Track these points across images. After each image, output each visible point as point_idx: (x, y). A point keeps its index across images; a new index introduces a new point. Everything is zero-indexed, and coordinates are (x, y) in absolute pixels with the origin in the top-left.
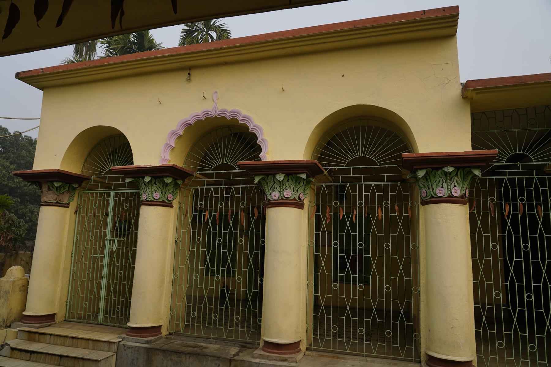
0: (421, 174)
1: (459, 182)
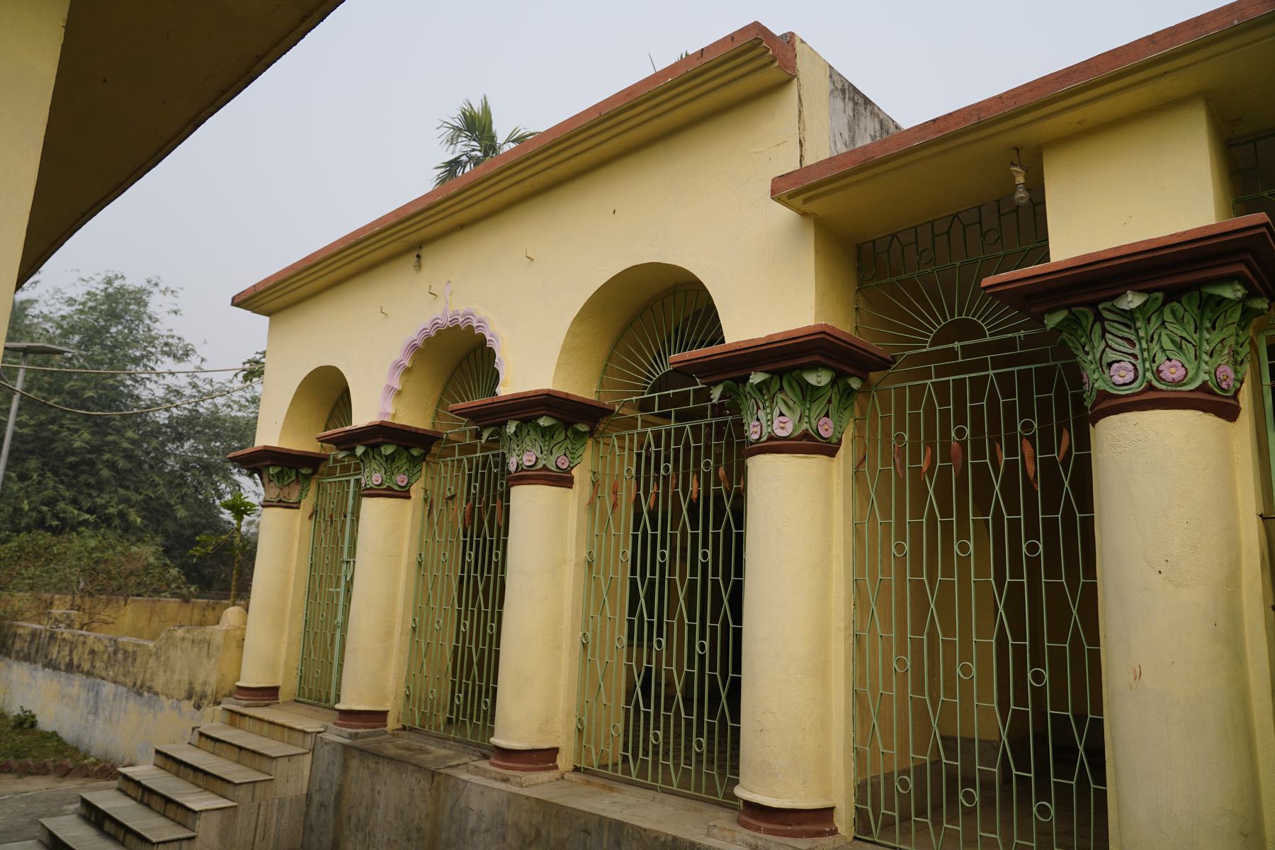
1: (791, 403)
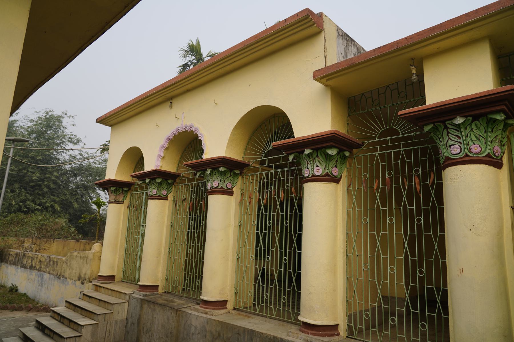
0: (147, 181)
1: (321, 162)
